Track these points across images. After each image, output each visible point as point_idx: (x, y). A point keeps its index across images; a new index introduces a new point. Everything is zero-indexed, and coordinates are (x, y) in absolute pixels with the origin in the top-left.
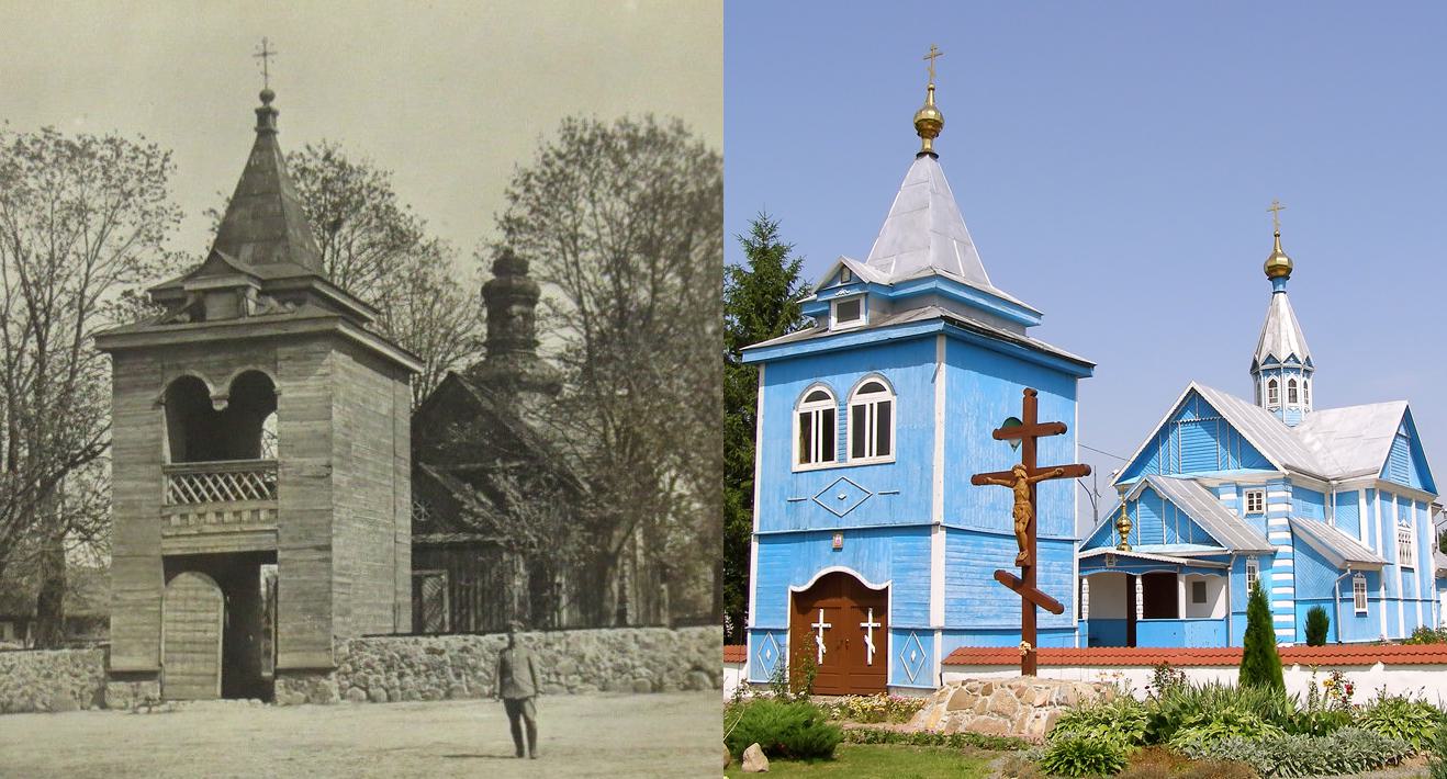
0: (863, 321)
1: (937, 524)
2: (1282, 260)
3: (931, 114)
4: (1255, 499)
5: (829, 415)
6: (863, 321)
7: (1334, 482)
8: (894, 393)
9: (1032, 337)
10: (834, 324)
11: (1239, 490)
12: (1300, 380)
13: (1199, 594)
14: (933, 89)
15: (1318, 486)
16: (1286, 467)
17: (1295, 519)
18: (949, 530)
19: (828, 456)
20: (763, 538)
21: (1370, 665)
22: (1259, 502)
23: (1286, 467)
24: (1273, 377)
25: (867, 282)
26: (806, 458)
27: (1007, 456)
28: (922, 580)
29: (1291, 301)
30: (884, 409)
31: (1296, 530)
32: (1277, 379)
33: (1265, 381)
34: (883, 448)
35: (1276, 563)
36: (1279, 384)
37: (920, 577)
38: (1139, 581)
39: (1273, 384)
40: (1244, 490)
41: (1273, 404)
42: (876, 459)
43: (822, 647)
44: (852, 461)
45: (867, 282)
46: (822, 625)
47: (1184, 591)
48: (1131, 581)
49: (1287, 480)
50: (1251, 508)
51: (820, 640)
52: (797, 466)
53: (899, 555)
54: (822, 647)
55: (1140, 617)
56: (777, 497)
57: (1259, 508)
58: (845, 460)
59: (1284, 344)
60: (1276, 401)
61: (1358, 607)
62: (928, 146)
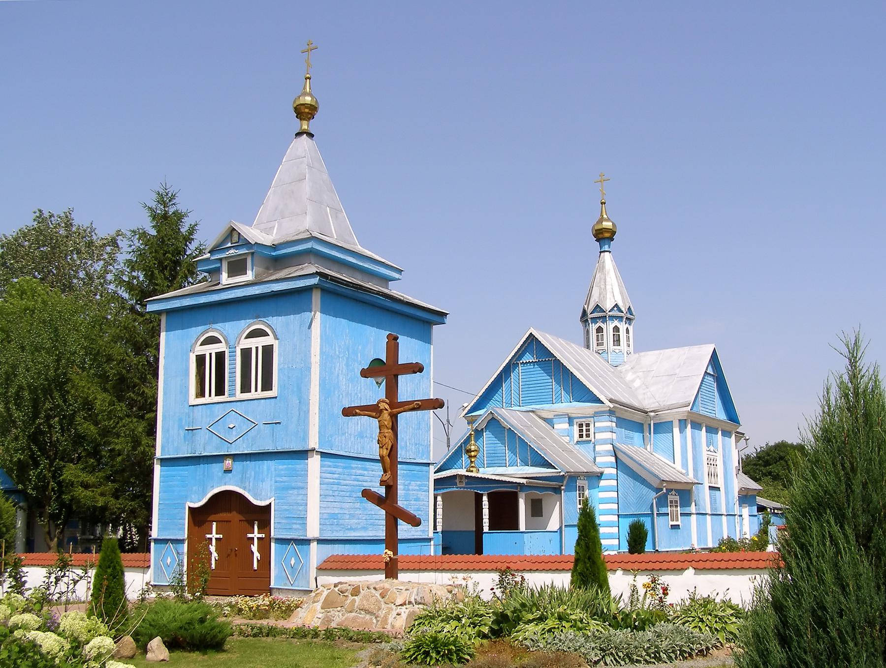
0: (249, 276)
1: (313, 450)
2: (607, 224)
3: (308, 99)
4: (584, 428)
5: (220, 357)
6: (249, 276)
7: (652, 414)
8: (276, 338)
9: (394, 290)
10: (225, 279)
11: (571, 421)
12: (623, 326)
13: (537, 509)
14: (310, 78)
15: (638, 417)
16: (611, 401)
17: (618, 445)
18: (324, 455)
19: (220, 391)
20: (164, 462)
21: (682, 570)
22: (588, 430)
23: (611, 401)
24: (600, 324)
25: (253, 243)
26: (201, 393)
27: (373, 392)
28: (300, 497)
29: (615, 259)
30: (268, 351)
31: (620, 455)
32: (603, 326)
33: (593, 328)
34: (267, 385)
35: (603, 483)
36: (605, 330)
37: (298, 495)
38: (485, 498)
39: (599, 330)
40: (575, 421)
41: (600, 348)
42: (260, 394)
43: (215, 555)
44: (240, 396)
45: (253, 243)
46: (214, 535)
47: (317, 498)
48: (479, 498)
49: (611, 412)
50: (581, 436)
51: (213, 548)
52: (193, 400)
53: (280, 476)
54: (215, 555)
55: (486, 529)
56: (176, 426)
57: (588, 436)
58: (234, 395)
59: (609, 295)
60: (602, 344)
61: (672, 520)
62: (305, 127)
